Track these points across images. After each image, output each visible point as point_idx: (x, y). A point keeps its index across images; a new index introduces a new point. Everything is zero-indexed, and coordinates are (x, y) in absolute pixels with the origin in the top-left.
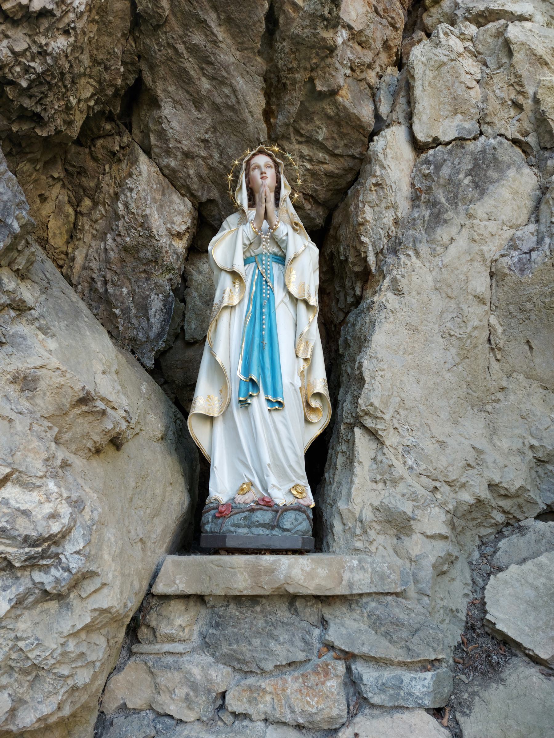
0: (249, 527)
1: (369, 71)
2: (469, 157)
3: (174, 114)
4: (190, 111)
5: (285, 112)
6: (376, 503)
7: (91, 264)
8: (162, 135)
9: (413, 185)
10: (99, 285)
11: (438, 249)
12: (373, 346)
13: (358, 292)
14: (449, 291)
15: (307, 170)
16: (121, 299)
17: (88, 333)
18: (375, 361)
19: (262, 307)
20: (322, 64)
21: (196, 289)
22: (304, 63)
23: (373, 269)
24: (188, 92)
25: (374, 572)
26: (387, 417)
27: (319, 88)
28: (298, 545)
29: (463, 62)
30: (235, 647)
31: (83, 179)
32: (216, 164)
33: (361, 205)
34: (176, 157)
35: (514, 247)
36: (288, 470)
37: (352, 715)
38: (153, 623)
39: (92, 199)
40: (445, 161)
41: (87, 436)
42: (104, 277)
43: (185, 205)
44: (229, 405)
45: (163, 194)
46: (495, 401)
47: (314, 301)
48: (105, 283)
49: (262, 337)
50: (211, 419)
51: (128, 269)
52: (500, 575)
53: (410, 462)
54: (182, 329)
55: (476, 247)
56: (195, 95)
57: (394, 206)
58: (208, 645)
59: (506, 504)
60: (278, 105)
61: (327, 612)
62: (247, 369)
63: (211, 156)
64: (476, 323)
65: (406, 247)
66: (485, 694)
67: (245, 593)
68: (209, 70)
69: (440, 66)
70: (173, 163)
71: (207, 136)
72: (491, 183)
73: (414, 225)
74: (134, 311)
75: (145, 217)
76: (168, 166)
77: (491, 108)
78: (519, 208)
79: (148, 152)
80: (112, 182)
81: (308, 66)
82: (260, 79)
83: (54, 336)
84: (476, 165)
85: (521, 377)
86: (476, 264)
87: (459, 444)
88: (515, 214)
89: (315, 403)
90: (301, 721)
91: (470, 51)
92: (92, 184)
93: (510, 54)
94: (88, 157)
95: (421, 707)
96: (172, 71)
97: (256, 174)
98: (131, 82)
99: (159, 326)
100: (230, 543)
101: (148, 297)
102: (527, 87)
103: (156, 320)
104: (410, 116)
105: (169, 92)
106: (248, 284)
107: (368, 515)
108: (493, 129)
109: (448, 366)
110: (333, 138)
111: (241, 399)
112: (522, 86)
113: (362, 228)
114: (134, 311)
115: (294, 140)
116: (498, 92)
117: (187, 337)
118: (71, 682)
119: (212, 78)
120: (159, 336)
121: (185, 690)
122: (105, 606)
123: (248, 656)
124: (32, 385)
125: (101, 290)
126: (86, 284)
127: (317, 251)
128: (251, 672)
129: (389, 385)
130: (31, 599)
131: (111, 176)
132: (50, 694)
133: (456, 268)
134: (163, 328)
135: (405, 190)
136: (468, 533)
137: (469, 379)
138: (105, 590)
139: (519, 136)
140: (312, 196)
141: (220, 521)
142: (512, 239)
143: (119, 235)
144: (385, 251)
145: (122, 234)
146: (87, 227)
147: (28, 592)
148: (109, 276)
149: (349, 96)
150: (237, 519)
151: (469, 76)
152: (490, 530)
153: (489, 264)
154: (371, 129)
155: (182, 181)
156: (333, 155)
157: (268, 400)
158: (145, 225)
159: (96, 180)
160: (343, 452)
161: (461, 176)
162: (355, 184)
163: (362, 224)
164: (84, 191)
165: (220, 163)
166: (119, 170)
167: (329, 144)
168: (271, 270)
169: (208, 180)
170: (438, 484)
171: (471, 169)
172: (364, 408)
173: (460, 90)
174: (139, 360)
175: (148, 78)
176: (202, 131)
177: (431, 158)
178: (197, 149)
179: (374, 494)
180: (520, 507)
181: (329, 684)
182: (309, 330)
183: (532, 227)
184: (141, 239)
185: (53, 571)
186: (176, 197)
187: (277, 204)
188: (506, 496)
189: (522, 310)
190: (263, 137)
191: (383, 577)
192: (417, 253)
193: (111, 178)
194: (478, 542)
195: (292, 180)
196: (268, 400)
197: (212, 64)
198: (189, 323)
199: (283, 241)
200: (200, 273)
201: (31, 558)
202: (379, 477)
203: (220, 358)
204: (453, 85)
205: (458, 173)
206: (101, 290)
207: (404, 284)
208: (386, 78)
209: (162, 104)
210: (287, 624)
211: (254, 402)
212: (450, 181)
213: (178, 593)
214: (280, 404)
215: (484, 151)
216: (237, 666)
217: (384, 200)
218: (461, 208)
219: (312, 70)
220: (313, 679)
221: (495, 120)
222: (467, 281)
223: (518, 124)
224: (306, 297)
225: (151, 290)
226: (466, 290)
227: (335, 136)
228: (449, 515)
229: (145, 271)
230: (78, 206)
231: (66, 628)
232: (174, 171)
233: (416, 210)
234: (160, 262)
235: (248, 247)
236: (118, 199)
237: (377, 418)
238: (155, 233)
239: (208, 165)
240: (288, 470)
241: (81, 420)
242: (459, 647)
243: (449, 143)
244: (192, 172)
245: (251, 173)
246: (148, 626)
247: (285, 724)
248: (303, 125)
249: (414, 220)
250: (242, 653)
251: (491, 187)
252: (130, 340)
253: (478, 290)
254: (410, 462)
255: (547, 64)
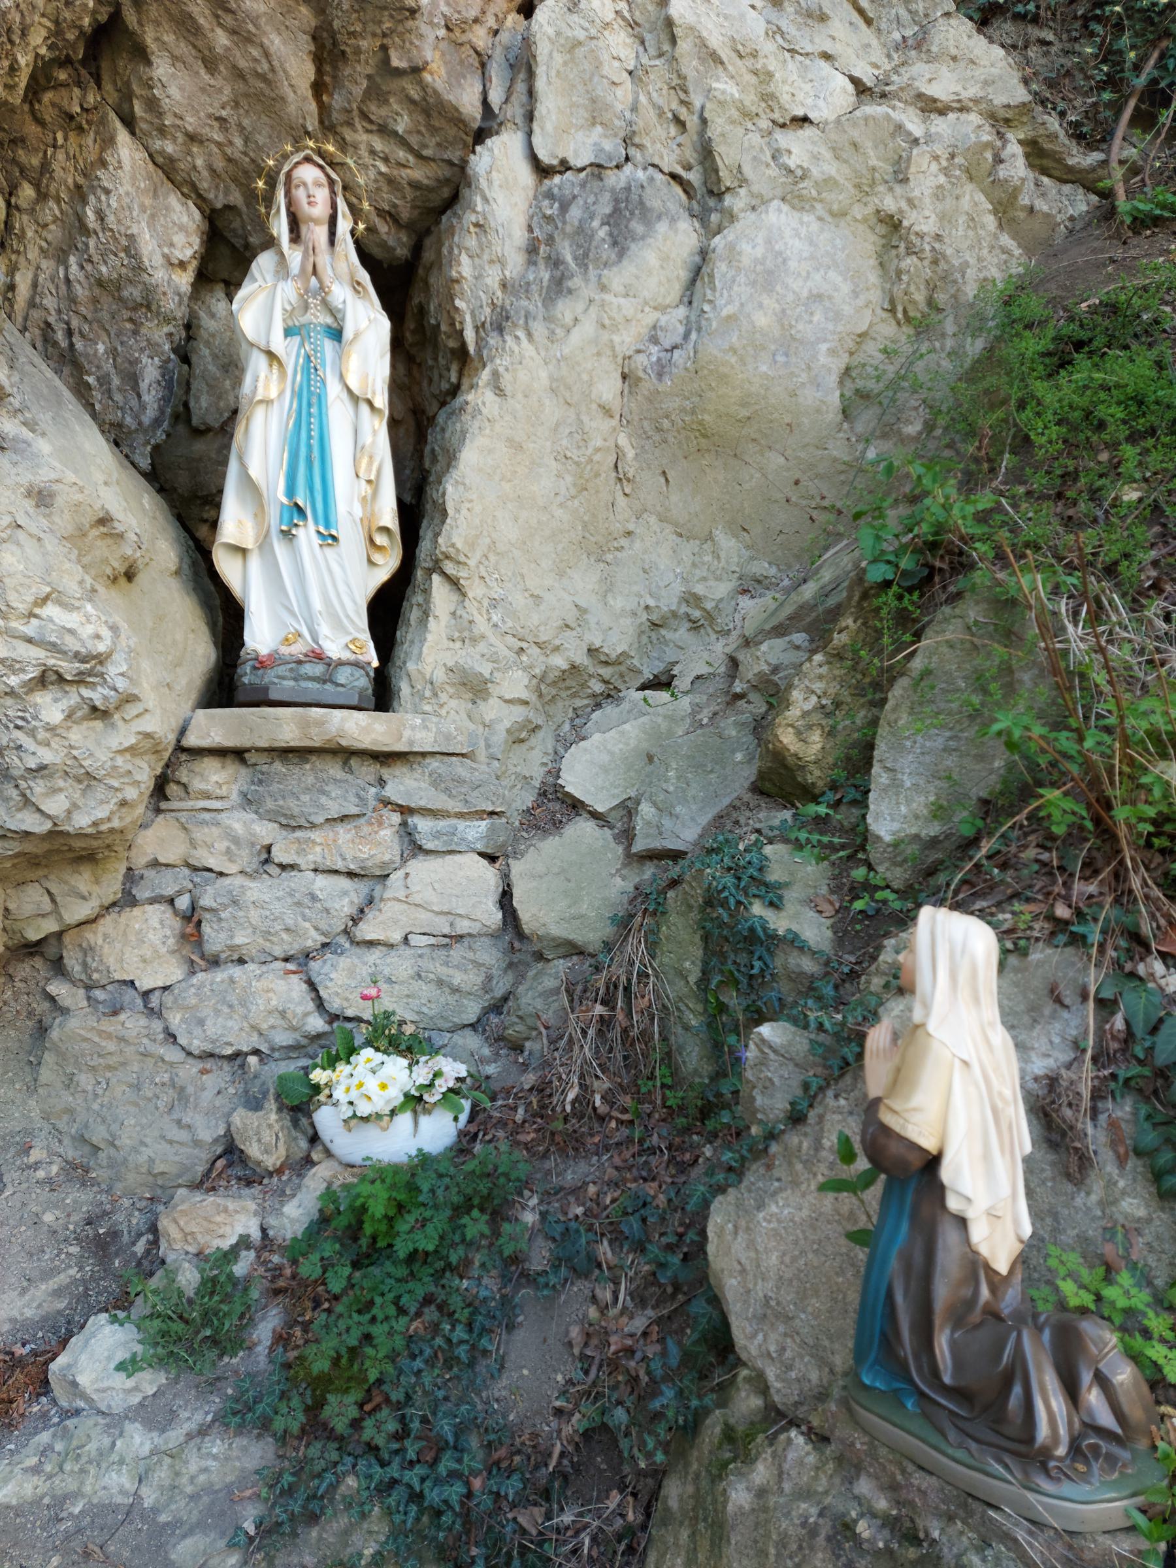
0: (296, 680)
1: (476, 27)
2: (607, 195)
3: (173, 75)
4: (197, 73)
5: (344, 92)
6: (450, 664)
7: (45, 302)
8: (152, 104)
9: (530, 229)
10: (60, 336)
11: (558, 331)
12: (461, 467)
13: (454, 379)
14: (568, 395)
15: (381, 173)
16: (96, 362)
17: (77, 428)
18: (461, 488)
19: (310, 405)
20: (400, 28)
21: (208, 344)
22: (371, 27)
23: (472, 349)
24: (195, 47)
25: (439, 732)
26: (472, 563)
27: (395, 62)
28: (355, 701)
29: (610, 38)
30: (281, 803)
31: (21, 152)
32: (237, 155)
33: (456, 251)
34: (174, 139)
35: (654, 340)
36: (345, 621)
37: (404, 861)
38: (184, 780)
39: (37, 186)
40: (575, 197)
41: (106, 561)
42: (68, 323)
43: (190, 215)
44: (267, 535)
45: (155, 196)
46: (617, 549)
47: (381, 400)
48: (69, 333)
49: (310, 447)
50: (243, 551)
51: (105, 315)
52: (582, 743)
53: (495, 618)
54: (186, 405)
55: (605, 336)
56: (207, 52)
57: (501, 261)
58: (250, 802)
59: (606, 672)
60: (334, 77)
61: (385, 773)
62: (291, 491)
63: (231, 143)
64: (599, 443)
65: (515, 325)
66: (540, 845)
67: (292, 744)
68: (228, 20)
69: (573, 47)
70: (170, 148)
71: (224, 113)
72: (633, 240)
73: (527, 291)
74: (116, 381)
75: (131, 237)
76: (162, 153)
77: (641, 123)
78: (669, 281)
79: (129, 123)
80: (70, 165)
81: (379, 31)
82: (307, 38)
83: (43, 434)
84: (616, 210)
85: (653, 520)
86: (604, 360)
87: (559, 600)
88: (662, 290)
89: (380, 540)
90: (352, 867)
91: (624, 18)
92: (35, 161)
93: (673, 40)
94: (28, 118)
95: (473, 850)
96: (170, 14)
97: (300, 194)
98: (103, 18)
99: (156, 406)
100: (274, 695)
101: (137, 361)
102: (692, 96)
103: (151, 397)
104: (530, 117)
105: (164, 43)
106: (290, 370)
107: (440, 676)
108: (643, 155)
109: (560, 499)
110: (419, 132)
111: (284, 528)
112: (686, 92)
113: (456, 286)
114: (116, 381)
115: (359, 127)
116: (654, 95)
117: (195, 421)
118: (120, 796)
119: (233, 32)
120: (157, 422)
121: (226, 844)
122: (149, 730)
123: (296, 811)
124: (48, 500)
125: (64, 344)
126: (37, 332)
127: (384, 325)
128: (300, 827)
129: (477, 521)
130: (79, 714)
131: (67, 153)
132: (102, 802)
133: (578, 364)
134: (162, 411)
135: (519, 236)
136: (560, 704)
137: (586, 518)
138: (147, 716)
139: (679, 170)
140: (389, 213)
141: (260, 672)
142: (654, 327)
143: (90, 261)
144: (488, 325)
145: (95, 259)
146: (30, 234)
147: (78, 707)
148: (75, 323)
149: (443, 72)
150: (281, 670)
151: (616, 64)
152: (586, 702)
153: (620, 360)
154: (476, 125)
155: (184, 175)
156: (419, 156)
157: (319, 532)
158: (130, 248)
159: (41, 155)
160: (419, 605)
161: (596, 223)
162: (449, 212)
163: (457, 281)
164: (22, 172)
165: (245, 154)
166: (81, 146)
167: (414, 140)
168: (323, 353)
169: (224, 175)
170: (524, 645)
171: (610, 215)
172: (444, 549)
173: (601, 89)
174: (127, 456)
175: (130, 17)
176: (216, 105)
177: (556, 190)
178: (208, 129)
179: (449, 654)
180: (622, 676)
181: (382, 833)
182: (374, 442)
183: (682, 311)
184: (124, 271)
185: (99, 689)
186: (174, 200)
187: (332, 241)
188: (606, 663)
189: (659, 430)
190: (312, 124)
191: (448, 737)
192: (529, 335)
193: (68, 158)
194: (571, 714)
195: (355, 211)
196: (319, 532)
197: (233, 12)
198: (198, 399)
199: (339, 311)
200: (213, 316)
201: (81, 673)
202: (457, 635)
203: (255, 472)
204: (591, 80)
205: (592, 218)
206: (64, 344)
207: (506, 381)
208: (504, 37)
209: (153, 58)
210: (340, 781)
211: (300, 533)
212: (580, 230)
213: (214, 745)
214: (334, 538)
215: (628, 189)
216: (284, 822)
217: (487, 251)
218: (592, 273)
219: (384, 35)
220: (366, 830)
221: (646, 142)
222: (591, 384)
223: (678, 151)
224: (369, 396)
225: (142, 350)
226: (589, 395)
227: (423, 129)
228: (535, 681)
229: (131, 320)
230: (11, 194)
231: (115, 746)
232: (171, 160)
233: (532, 268)
234: (154, 307)
235: (289, 314)
236: (84, 201)
237: (459, 563)
238: (147, 263)
239: (225, 154)
240: (345, 621)
241: (99, 543)
242: (528, 811)
243: (583, 169)
244: (199, 162)
245: (293, 191)
246: (178, 783)
247: (336, 872)
248: (373, 108)
249: (528, 284)
250: (289, 809)
251: (633, 246)
252: (111, 424)
253: (605, 397)
254: (495, 618)
255: (722, 63)
